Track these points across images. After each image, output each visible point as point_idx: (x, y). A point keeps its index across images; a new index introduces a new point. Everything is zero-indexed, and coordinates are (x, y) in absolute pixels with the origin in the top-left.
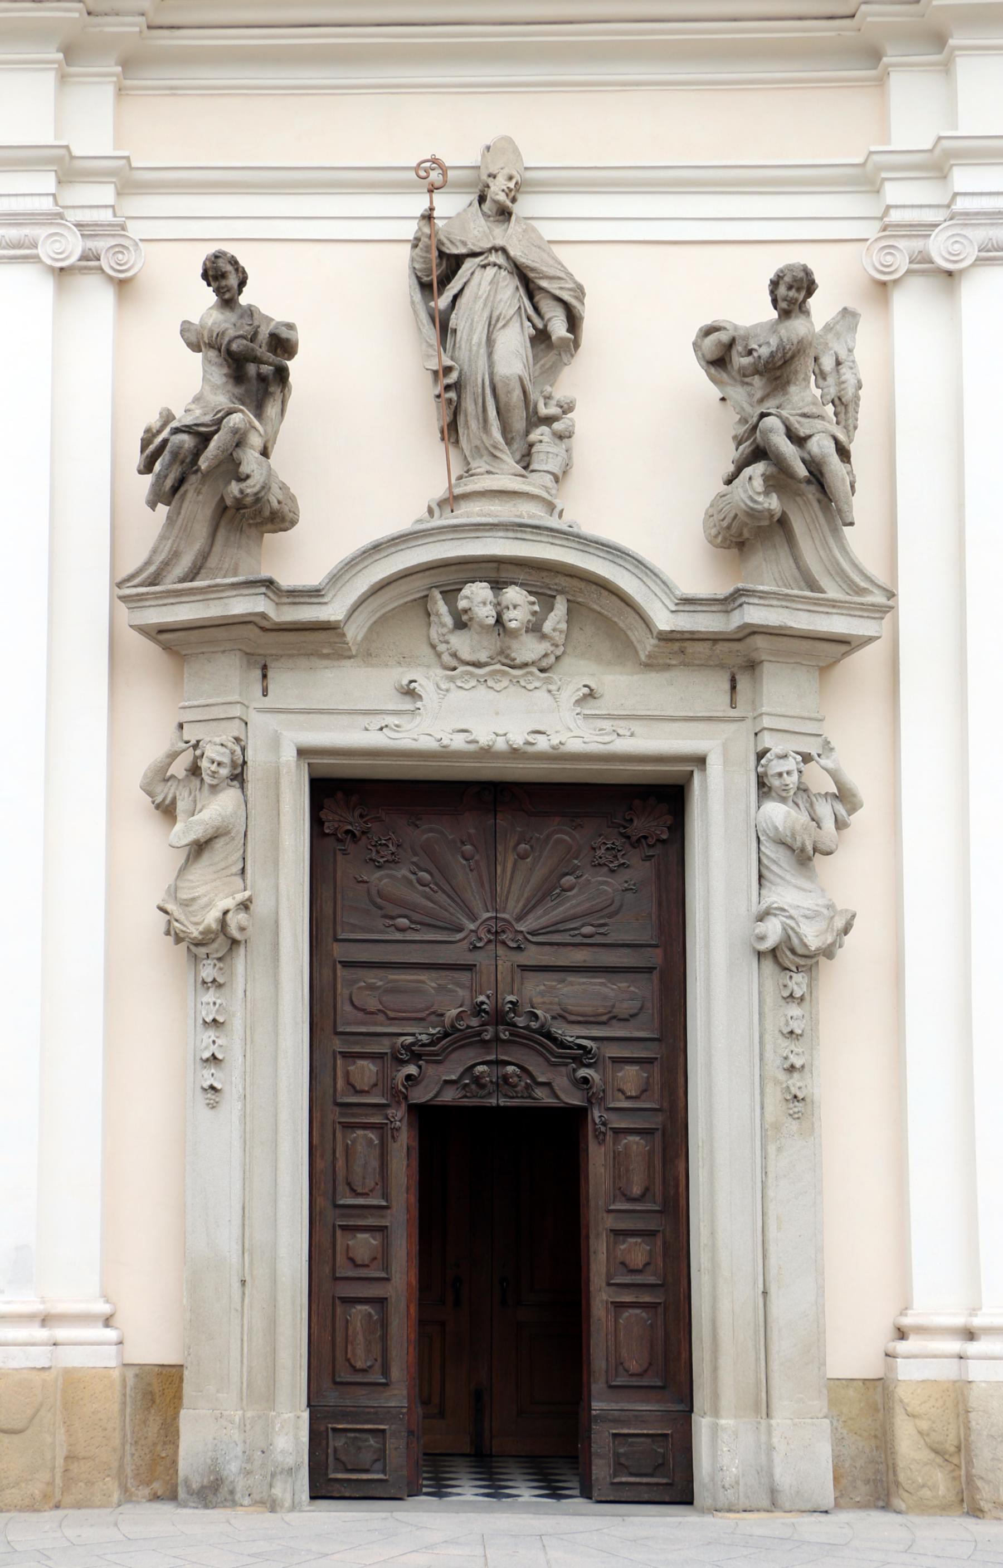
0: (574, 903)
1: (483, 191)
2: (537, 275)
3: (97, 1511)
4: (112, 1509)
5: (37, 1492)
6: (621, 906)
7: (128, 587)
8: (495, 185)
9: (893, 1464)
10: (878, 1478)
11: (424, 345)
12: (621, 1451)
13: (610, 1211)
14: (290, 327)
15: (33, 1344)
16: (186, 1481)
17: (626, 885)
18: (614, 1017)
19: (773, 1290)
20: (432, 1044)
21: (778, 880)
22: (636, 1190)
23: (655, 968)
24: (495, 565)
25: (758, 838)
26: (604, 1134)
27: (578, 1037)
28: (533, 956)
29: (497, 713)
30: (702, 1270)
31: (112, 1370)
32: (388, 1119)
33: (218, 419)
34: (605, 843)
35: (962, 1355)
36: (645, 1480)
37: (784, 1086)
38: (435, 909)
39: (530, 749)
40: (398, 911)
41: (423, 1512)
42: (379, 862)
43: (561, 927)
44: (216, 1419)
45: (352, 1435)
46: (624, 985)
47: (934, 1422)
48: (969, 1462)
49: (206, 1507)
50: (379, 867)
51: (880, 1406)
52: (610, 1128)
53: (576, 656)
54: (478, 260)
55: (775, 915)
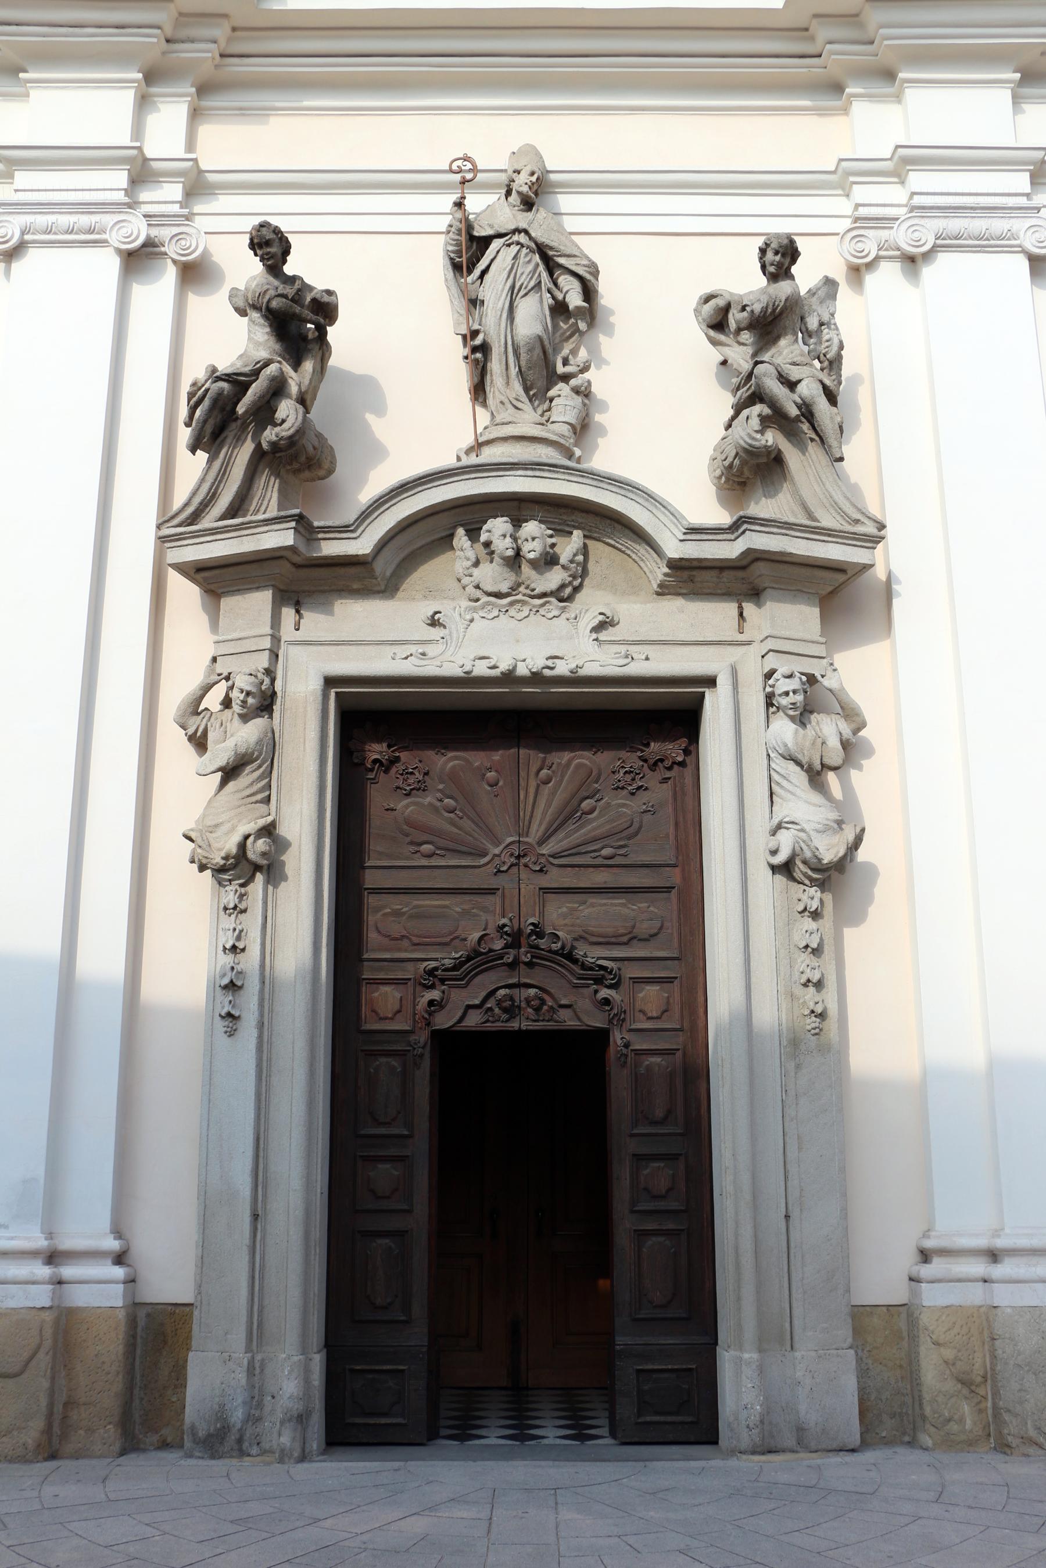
0: (595, 825)
1: (508, 186)
2: (555, 253)
3: (94, 1462)
4: (111, 1460)
5: (30, 1441)
6: (640, 828)
7: (168, 527)
8: (519, 179)
9: (919, 1396)
10: (904, 1411)
11: (456, 315)
12: (646, 1388)
13: (632, 1135)
14: (329, 293)
15: (34, 1283)
16: (193, 1427)
17: (644, 807)
18: (635, 938)
19: (795, 1214)
20: (455, 968)
21: (789, 796)
22: (659, 1113)
23: (674, 887)
24: (516, 503)
25: (769, 755)
26: (626, 1056)
27: (599, 958)
28: (556, 878)
29: (518, 641)
30: (724, 1194)
31: (118, 1310)
32: (411, 1046)
33: (257, 369)
34: (623, 767)
35: (986, 1278)
36: (669, 1419)
37: (801, 1001)
38: (460, 834)
39: (547, 673)
40: (425, 837)
41: (439, 1460)
42: (406, 790)
43: (583, 849)
44: (225, 1362)
45: (370, 1376)
46: (644, 905)
47: (959, 1351)
48: (996, 1394)
49: (213, 1457)
50: (406, 795)
51: (905, 1334)
52: (632, 1050)
53: (593, 587)
54: (502, 240)
55: (788, 829)
